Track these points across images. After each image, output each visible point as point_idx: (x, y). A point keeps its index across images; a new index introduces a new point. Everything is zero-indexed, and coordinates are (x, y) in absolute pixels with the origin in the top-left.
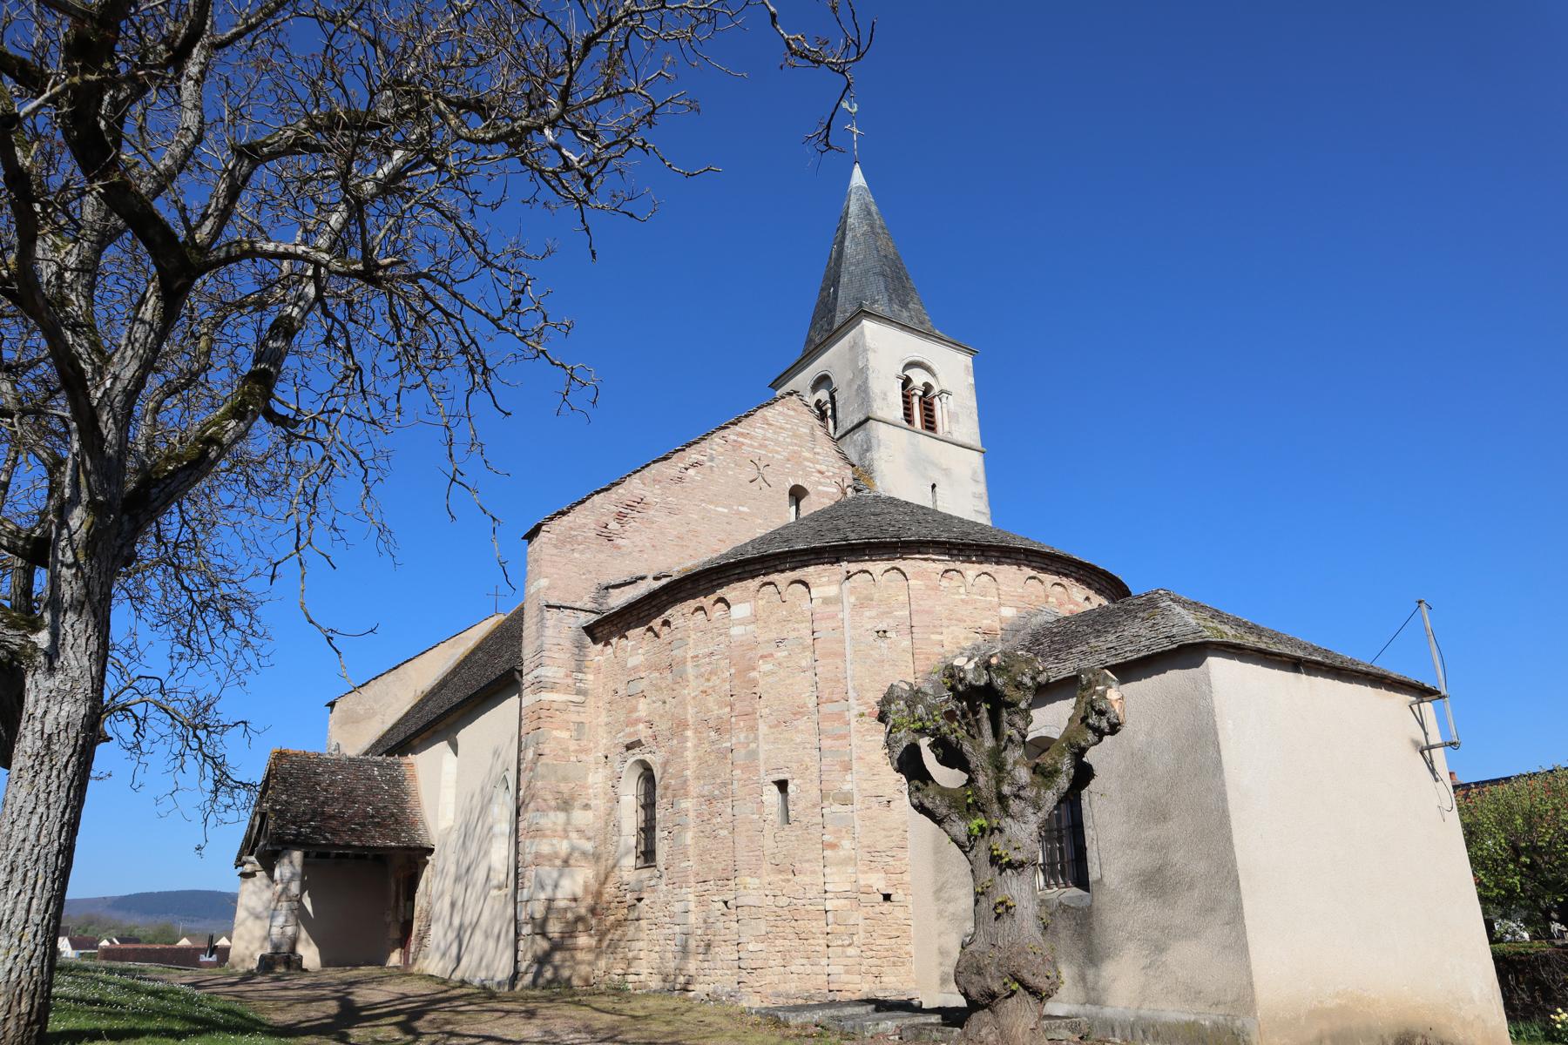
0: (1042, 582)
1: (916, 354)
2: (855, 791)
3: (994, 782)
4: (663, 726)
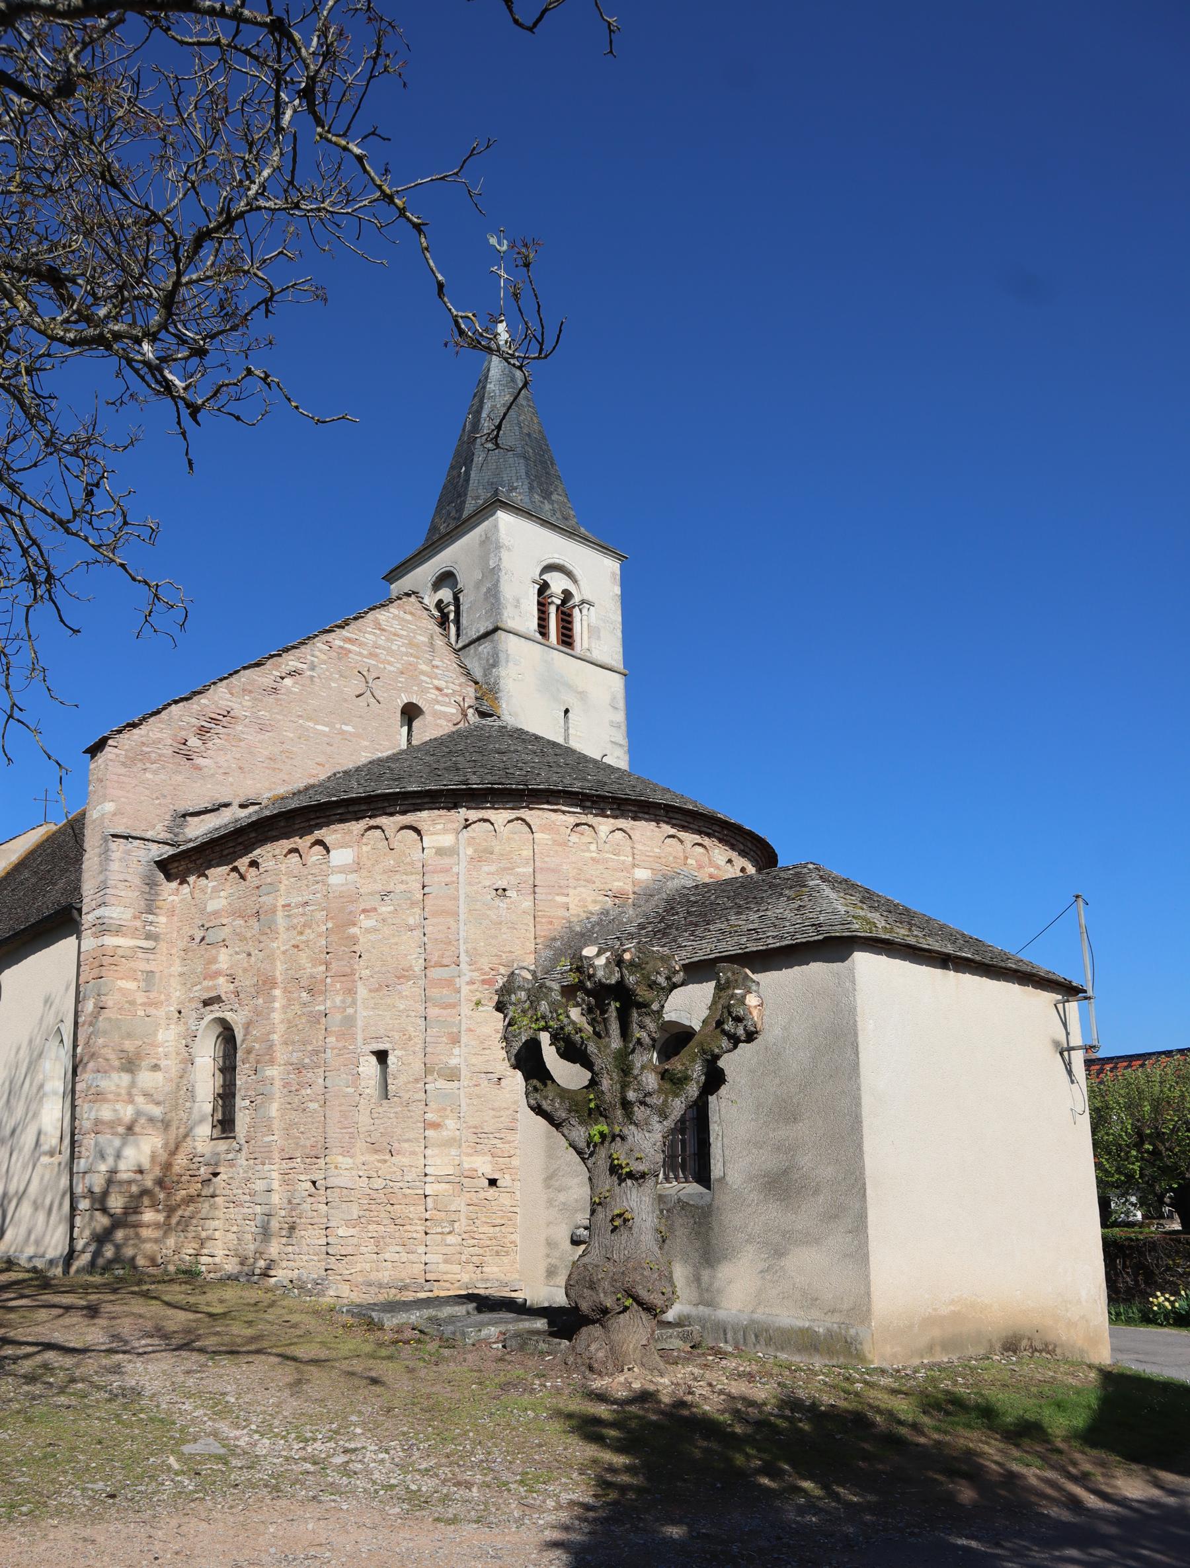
0: (681, 841)
1: (556, 556)
2: (463, 1067)
3: (618, 1086)
4: (247, 982)
